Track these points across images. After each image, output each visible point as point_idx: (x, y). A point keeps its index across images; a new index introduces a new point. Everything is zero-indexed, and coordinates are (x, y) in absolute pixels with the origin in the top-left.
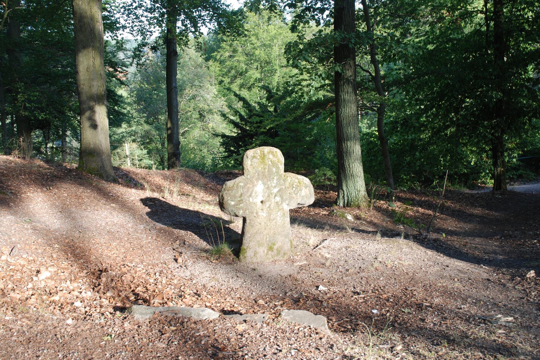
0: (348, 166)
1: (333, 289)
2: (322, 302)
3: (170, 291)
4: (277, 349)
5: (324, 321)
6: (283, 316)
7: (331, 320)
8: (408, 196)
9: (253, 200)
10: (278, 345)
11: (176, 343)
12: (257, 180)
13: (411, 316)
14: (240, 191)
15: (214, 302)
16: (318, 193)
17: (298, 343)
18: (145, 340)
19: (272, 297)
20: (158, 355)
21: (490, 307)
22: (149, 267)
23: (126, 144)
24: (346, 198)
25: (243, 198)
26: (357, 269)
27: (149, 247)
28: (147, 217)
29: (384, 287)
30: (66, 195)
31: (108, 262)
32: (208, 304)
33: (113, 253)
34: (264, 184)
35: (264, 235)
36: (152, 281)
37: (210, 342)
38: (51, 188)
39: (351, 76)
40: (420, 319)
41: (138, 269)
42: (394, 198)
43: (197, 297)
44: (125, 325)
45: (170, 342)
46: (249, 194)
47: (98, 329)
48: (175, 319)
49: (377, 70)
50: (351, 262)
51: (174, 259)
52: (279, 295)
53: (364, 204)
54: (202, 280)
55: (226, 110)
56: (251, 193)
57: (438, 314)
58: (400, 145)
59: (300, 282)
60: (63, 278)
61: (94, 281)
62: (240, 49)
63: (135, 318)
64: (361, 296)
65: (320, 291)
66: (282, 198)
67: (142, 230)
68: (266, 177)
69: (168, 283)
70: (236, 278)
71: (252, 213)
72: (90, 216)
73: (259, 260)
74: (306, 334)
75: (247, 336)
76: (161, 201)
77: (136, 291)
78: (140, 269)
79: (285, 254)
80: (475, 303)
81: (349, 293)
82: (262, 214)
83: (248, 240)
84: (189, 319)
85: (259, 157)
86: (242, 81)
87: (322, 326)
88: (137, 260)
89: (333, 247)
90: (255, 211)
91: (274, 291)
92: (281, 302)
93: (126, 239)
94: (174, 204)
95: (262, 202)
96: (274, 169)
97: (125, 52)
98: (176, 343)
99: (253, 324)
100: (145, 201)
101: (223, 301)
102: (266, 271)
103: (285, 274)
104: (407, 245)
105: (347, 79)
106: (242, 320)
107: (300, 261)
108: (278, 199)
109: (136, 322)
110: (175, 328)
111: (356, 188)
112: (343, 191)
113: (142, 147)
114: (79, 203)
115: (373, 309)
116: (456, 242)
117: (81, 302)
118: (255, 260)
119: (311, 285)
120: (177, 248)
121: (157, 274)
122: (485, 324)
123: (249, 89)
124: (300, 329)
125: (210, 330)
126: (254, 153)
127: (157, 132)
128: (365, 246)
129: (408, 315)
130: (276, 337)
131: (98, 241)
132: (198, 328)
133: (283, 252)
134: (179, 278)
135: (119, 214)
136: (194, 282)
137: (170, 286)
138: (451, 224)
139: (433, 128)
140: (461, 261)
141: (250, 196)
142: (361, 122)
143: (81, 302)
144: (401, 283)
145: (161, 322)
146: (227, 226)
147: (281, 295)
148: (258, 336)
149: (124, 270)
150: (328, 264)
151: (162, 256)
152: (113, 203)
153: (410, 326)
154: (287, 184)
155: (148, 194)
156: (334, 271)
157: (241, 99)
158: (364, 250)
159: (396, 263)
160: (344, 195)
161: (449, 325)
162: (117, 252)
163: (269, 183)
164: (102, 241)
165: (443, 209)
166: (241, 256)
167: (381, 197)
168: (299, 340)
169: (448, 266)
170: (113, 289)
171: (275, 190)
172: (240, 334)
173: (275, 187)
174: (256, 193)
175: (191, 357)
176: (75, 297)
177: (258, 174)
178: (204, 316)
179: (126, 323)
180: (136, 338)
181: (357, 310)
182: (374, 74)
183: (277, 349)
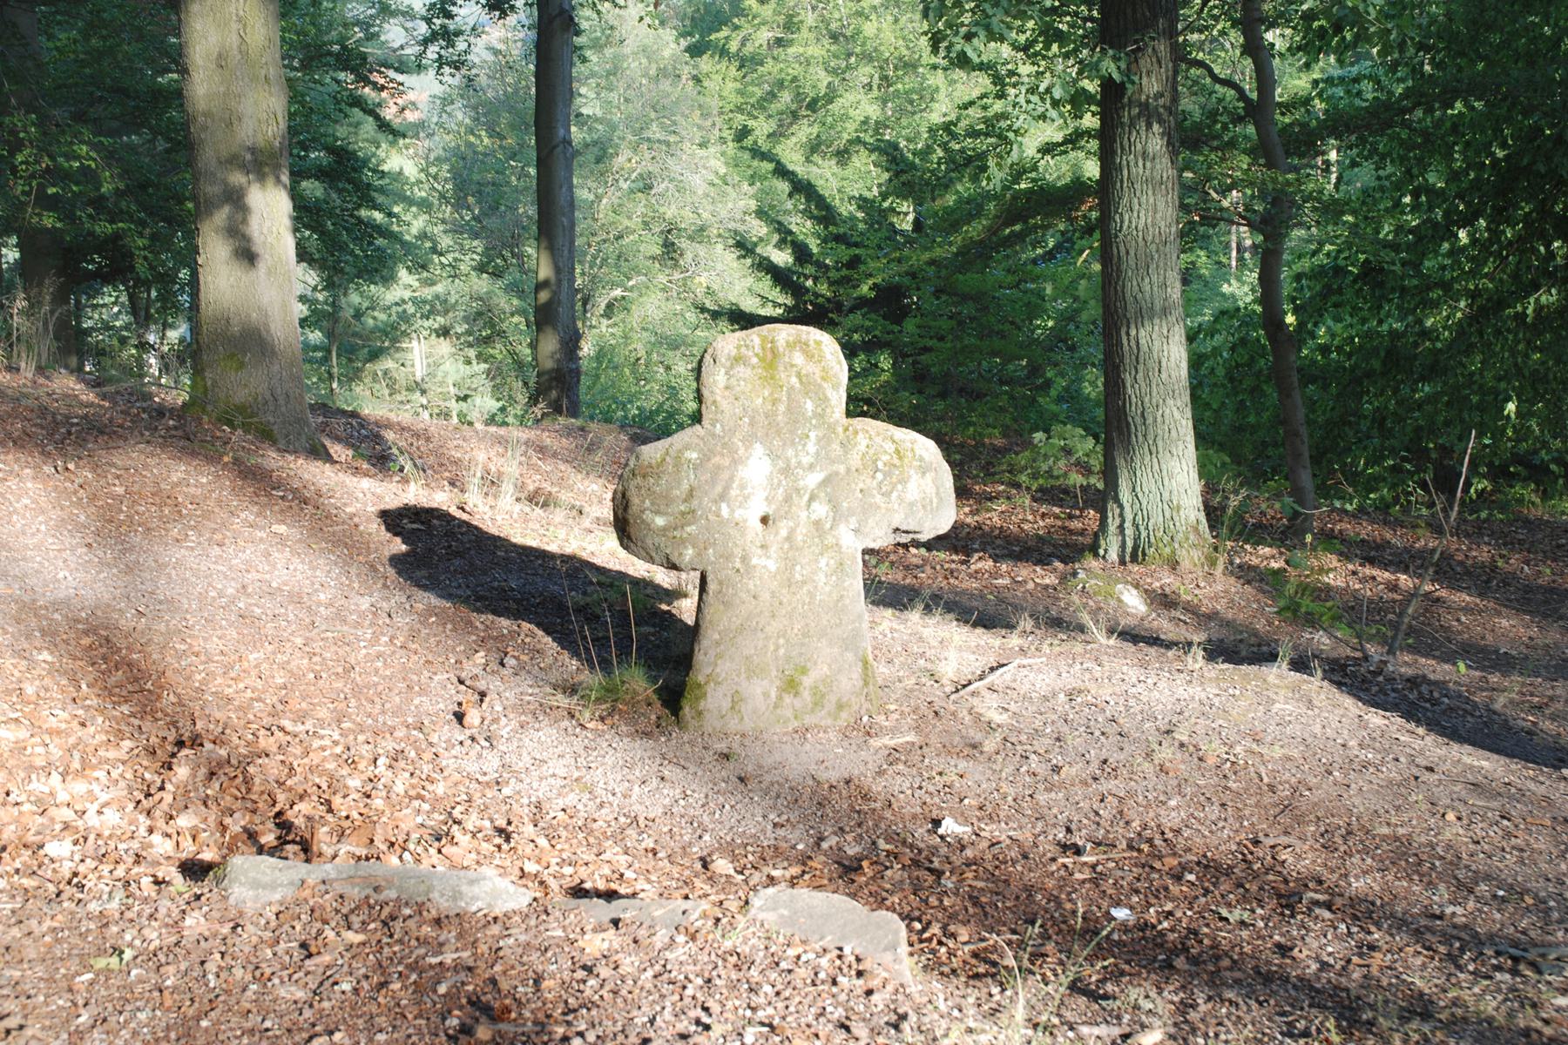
0: (1138, 420)
1: (989, 830)
2: (939, 874)
3: (410, 820)
4: (698, 1022)
5: (896, 932)
6: (753, 911)
7: (953, 936)
8: (1366, 530)
9: (733, 511)
10: (706, 1009)
11: (346, 986)
12: (749, 441)
13: (1245, 934)
14: (688, 479)
15: (554, 861)
16: (1043, 516)
17: (780, 1005)
18: (238, 973)
19: (769, 853)
20: (268, 1024)
21: (1555, 915)
22: (361, 738)
23: (415, 343)
24: (1129, 531)
25: (695, 503)
26: (1094, 768)
27: (377, 671)
28: (391, 572)
29: (1178, 832)
30: (120, 490)
31: (218, 715)
32: (531, 867)
33: (241, 686)
34: (773, 455)
35: (767, 638)
36: (354, 783)
37: (470, 988)
38: (71, 466)
39: (1160, 95)
40: (1279, 946)
41: (316, 743)
42: (1309, 538)
43: (498, 841)
44: (189, 922)
45: (327, 984)
46: (719, 489)
47: (88, 930)
48: (371, 907)
49: (1265, 79)
50: (1075, 741)
51: (455, 714)
52: (793, 847)
53: (1191, 558)
54: (535, 785)
55: (758, 229)
56: (727, 488)
57: (1349, 934)
58: (1350, 356)
59: (878, 805)
60: (40, 762)
61: (147, 776)
62: (810, 19)
63: (232, 901)
64: (1084, 859)
65: (942, 837)
66: (835, 507)
67: (362, 615)
68: (778, 433)
69: (412, 793)
70: (655, 782)
71: (728, 557)
72: (191, 561)
73: (748, 725)
74: (822, 975)
75: (605, 972)
76: (454, 518)
77: (290, 815)
78: (327, 742)
79: (840, 706)
80: (1503, 900)
81: (1047, 847)
82: (763, 561)
83: (712, 653)
84: (420, 908)
85: (755, 360)
86: (815, 130)
87: (885, 949)
88: (323, 713)
89: (1024, 689)
90: (738, 552)
91: (781, 832)
92: (795, 870)
93: (299, 641)
94: (494, 531)
95: (764, 520)
96: (809, 406)
97: (409, 25)
98: (346, 986)
99: (642, 933)
100: (394, 520)
101: (589, 857)
102: (768, 761)
103: (833, 776)
104: (1295, 689)
105: (1145, 107)
106: (606, 919)
107: (894, 731)
108: (821, 510)
109: (233, 913)
110: (360, 938)
111: (1166, 496)
112: (1121, 507)
113: (472, 353)
114: (160, 518)
115: (1118, 904)
116: (1506, 694)
117: (76, 843)
118: (733, 725)
119: (914, 817)
120: (475, 677)
121: (382, 761)
122: (1514, 972)
123: (843, 156)
124: (804, 958)
125: (483, 948)
126: (738, 347)
127: (515, 302)
128: (1140, 688)
129: (1242, 925)
130: (709, 981)
131: (198, 645)
132: (442, 939)
133: (833, 698)
134: (457, 777)
135: (296, 560)
136: (506, 791)
137: (416, 803)
138: (1510, 628)
139: (1474, 295)
140: (1488, 754)
141: (723, 497)
142: (1238, 279)
143: (76, 843)
144: (1241, 818)
145: (317, 914)
146: (664, 607)
147: (800, 847)
148: (650, 973)
149: (266, 742)
150: (990, 745)
151: (417, 701)
152: (283, 522)
153: (1231, 969)
154: (855, 460)
155: (415, 494)
156: (1009, 769)
157: (803, 188)
158: (1132, 702)
159: (1238, 749)
160: (1123, 521)
161: (1375, 971)
162: (259, 684)
163: (790, 452)
164: (214, 645)
165: (1488, 581)
166: (687, 710)
167: (1256, 533)
168: (787, 993)
169: (1431, 769)
170: (205, 804)
171: (812, 480)
172: (584, 967)
173: (811, 467)
174: (742, 487)
175: (381, 1037)
176: (58, 827)
177: (752, 418)
178: (475, 898)
179: (196, 914)
180: (211, 967)
181: (1059, 905)
182: (1254, 96)
183: (698, 1022)
